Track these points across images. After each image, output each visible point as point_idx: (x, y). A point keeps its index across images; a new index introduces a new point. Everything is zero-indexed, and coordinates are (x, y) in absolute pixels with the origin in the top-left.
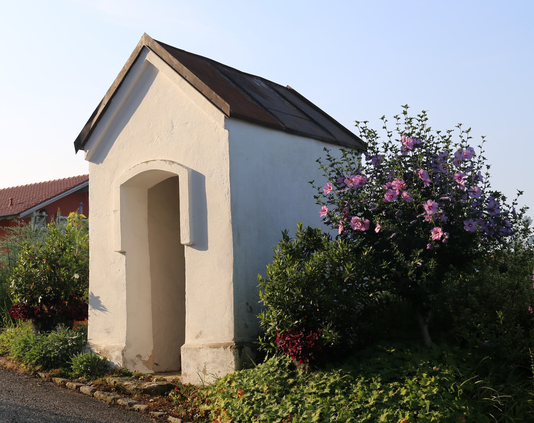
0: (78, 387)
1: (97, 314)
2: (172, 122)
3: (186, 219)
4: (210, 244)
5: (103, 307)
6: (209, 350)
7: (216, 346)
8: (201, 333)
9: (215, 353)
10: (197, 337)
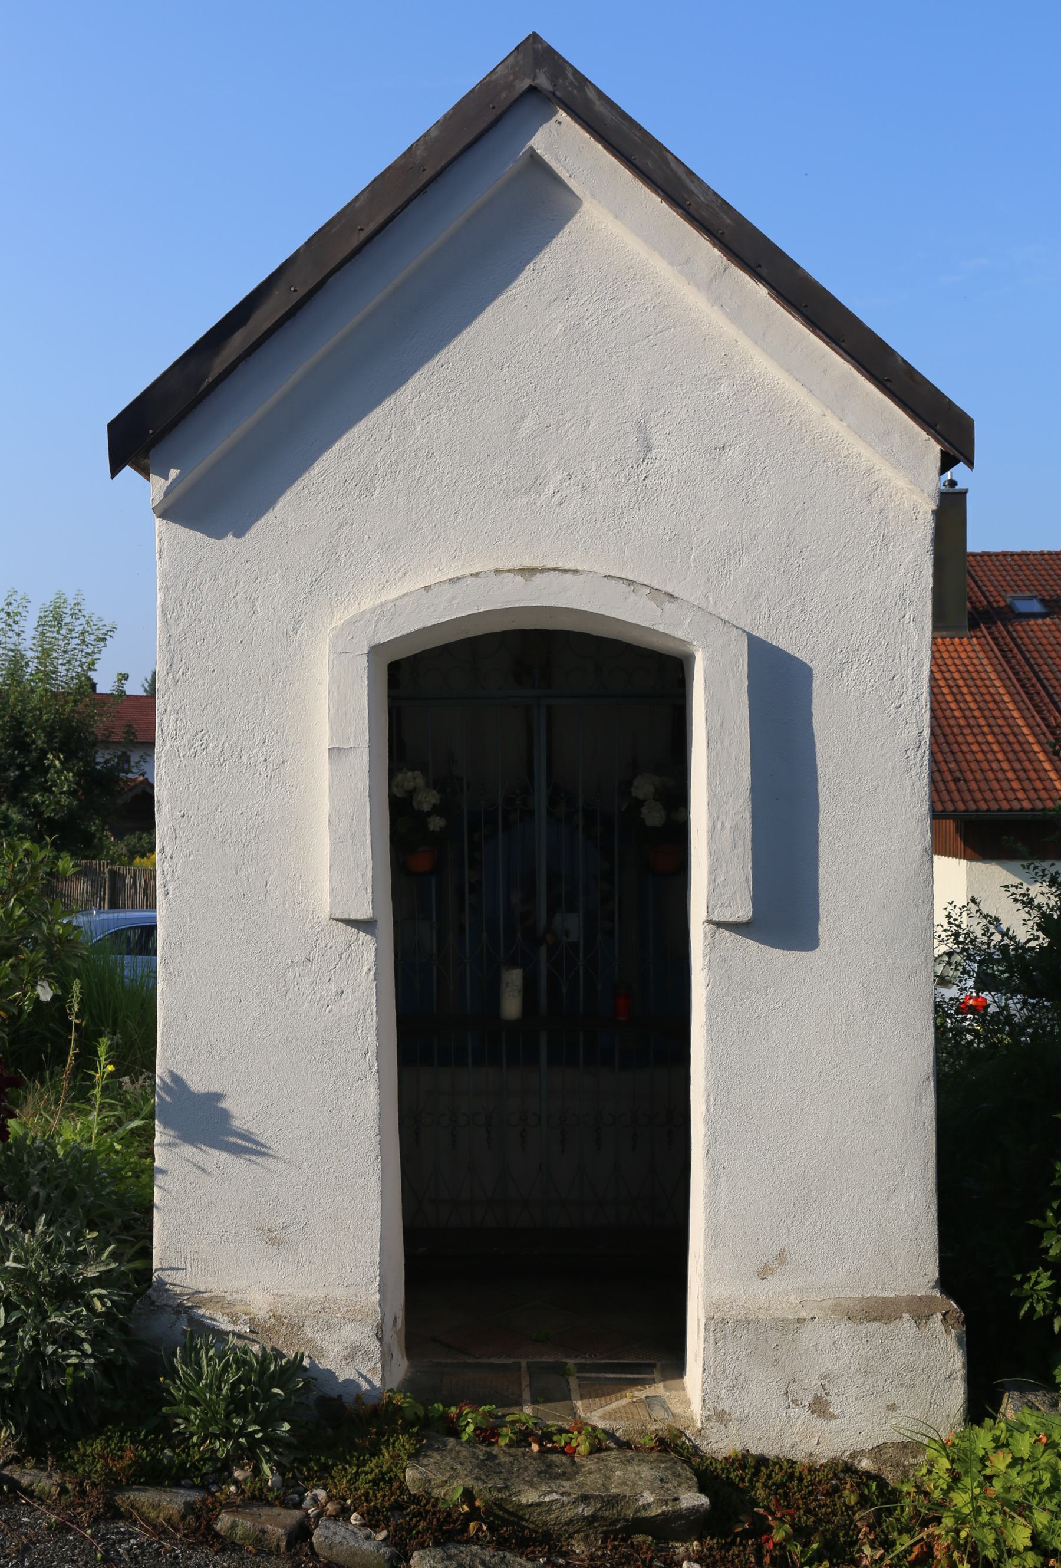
0: (302, 1533)
1: (211, 1166)
2: (642, 427)
3: (735, 828)
4: (823, 929)
5: (246, 1137)
6: (843, 1330)
7: (878, 1311)
8: (781, 1257)
9: (875, 1342)
10: (764, 1272)
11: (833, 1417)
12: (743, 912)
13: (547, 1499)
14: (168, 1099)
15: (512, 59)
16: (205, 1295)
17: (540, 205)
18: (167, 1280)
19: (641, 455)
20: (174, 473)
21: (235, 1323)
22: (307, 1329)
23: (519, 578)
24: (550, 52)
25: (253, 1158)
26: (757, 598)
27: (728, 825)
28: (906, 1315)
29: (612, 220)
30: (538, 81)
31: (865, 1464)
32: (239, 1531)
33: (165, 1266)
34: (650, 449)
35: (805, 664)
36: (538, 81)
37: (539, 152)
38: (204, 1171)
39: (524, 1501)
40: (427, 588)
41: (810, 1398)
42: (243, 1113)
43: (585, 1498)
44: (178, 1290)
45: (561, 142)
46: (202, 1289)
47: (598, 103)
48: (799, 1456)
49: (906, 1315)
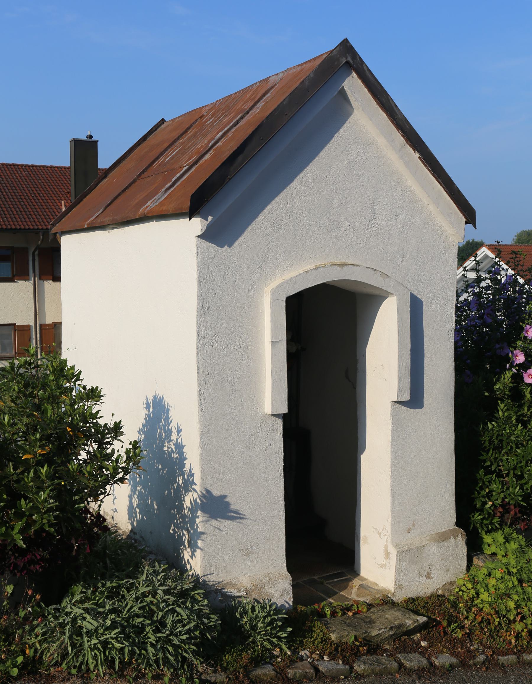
3: (406, 365)
5: (236, 512)
8: (413, 524)
11: (432, 578)
12: (407, 397)
13: (380, 632)
14: (205, 501)
15: (338, 47)
16: (223, 583)
17: (341, 108)
18: (207, 580)
19: (372, 217)
20: (210, 218)
21: (239, 592)
22: (266, 588)
23: (339, 268)
24: (351, 47)
25: (239, 520)
26: (407, 275)
27: (404, 364)
28: (452, 537)
29: (365, 119)
30: (345, 60)
31: (440, 592)
32: (298, 675)
33: (206, 574)
34: (375, 214)
35: (421, 300)
36: (345, 60)
37: (345, 89)
38: (220, 529)
39: (373, 635)
40: (307, 272)
41: (426, 573)
42: (235, 503)
43: (391, 628)
44: (212, 583)
45: (352, 85)
46: (221, 581)
47: (367, 72)
48: (422, 595)
49: (452, 537)
